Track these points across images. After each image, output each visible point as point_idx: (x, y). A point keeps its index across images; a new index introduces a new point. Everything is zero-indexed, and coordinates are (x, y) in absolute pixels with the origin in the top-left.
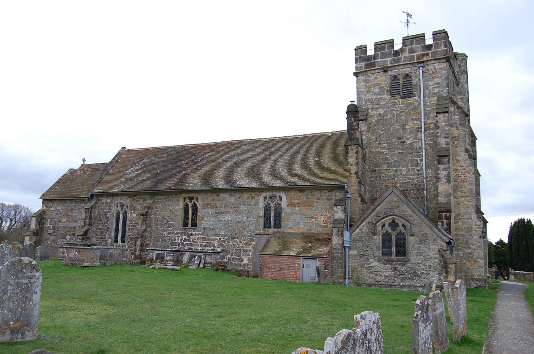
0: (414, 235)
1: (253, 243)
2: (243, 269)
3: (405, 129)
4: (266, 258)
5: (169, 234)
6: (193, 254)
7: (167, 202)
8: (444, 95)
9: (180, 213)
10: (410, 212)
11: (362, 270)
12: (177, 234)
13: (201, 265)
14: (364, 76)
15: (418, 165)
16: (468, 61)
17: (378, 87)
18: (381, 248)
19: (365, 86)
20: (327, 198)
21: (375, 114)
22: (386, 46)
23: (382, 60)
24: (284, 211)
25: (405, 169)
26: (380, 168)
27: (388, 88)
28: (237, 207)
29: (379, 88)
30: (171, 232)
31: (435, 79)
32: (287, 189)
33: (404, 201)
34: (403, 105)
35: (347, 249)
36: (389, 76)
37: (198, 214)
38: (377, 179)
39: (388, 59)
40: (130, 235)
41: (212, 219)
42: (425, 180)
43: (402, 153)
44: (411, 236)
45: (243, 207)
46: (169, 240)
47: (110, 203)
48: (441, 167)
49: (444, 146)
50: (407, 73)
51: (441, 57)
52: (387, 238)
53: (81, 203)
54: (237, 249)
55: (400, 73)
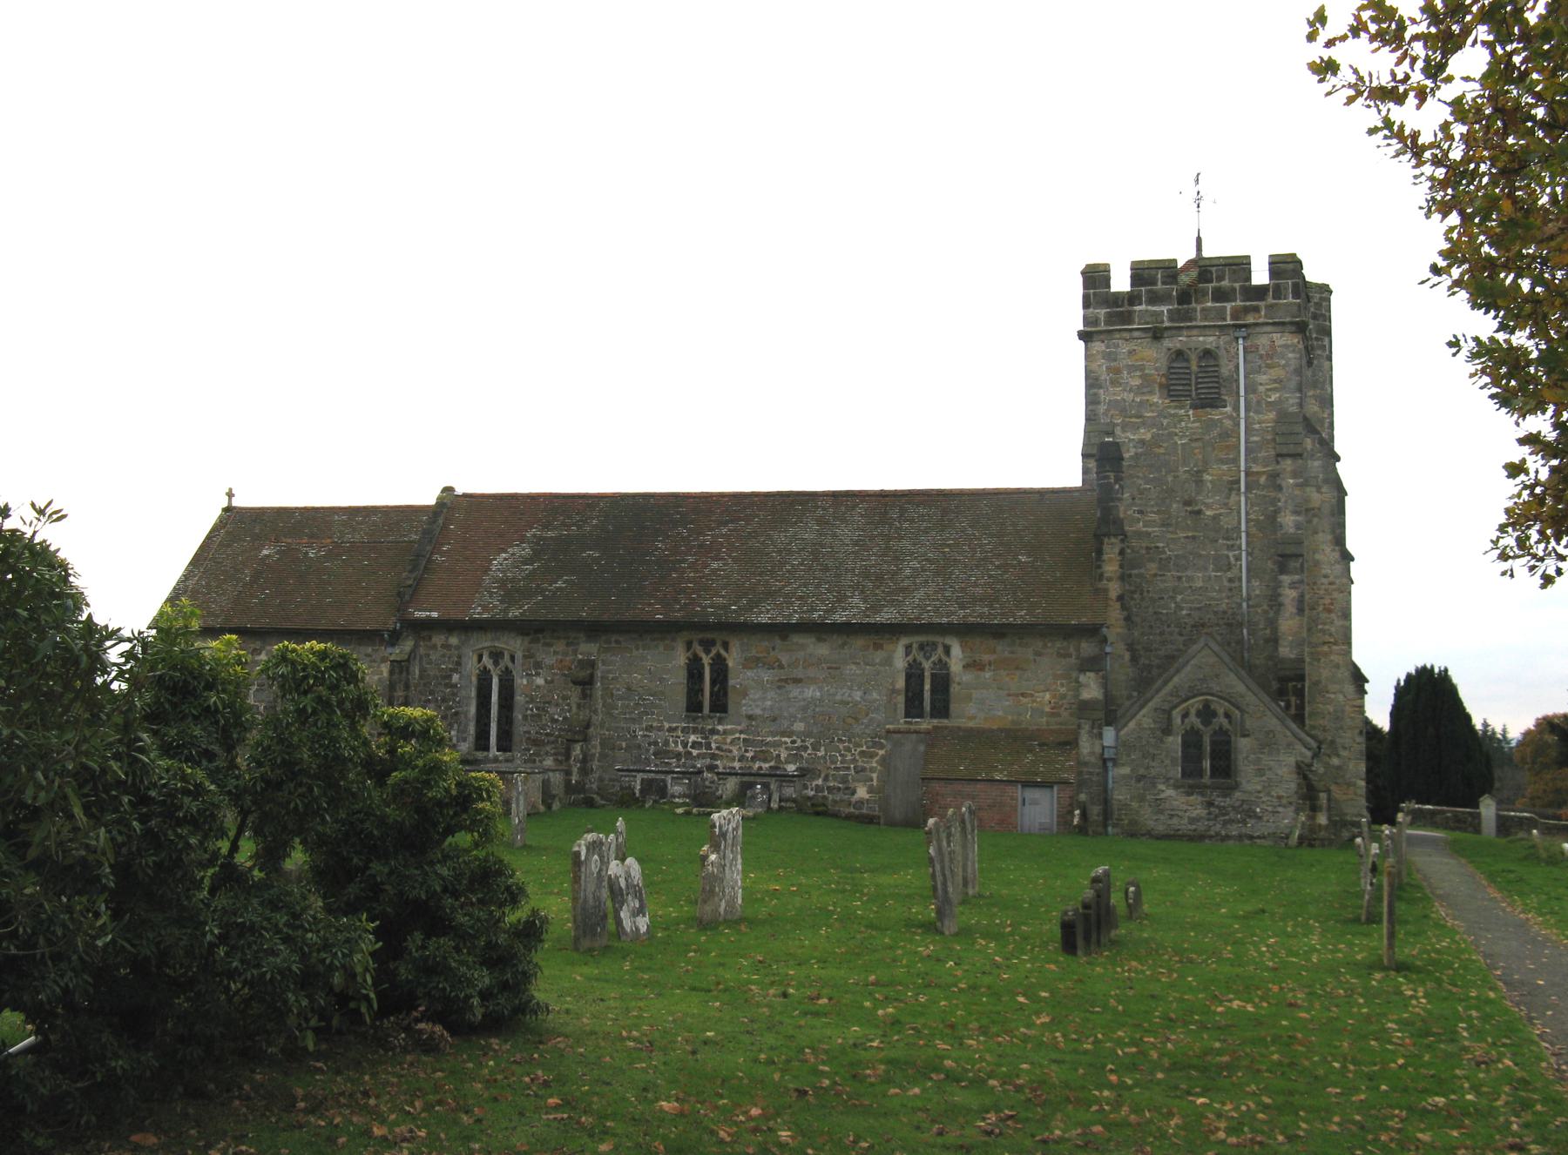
0: (1248, 736)
1: (881, 752)
2: (857, 812)
3: (1202, 481)
4: (936, 786)
5: (646, 730)
6: (746, 779)
7: (637, 649)
8: (1291, 409)
9: (676, 678)
10: (1241, 688)
11: (1140, 806)
12: (671, 730)
13: (774, 805)
14: (1103, 342)
15: (1229, 569)
16: (1333, 298)
17: (1138, 373)
18: (1180, 761)
19: (1107, 368)
20: (1058, 653)
21: (1130, 440)
22: (1159, 276)
23: (1150, 308)
24: (957, 679)
25: (1200, 575)
26: (1142, 571)
27: (1163, 380)
28: (836, 668)
29: (1141, 377)
30: (655, 724)
31: (1272, 371)
32: (964, 631)
33: (1231, 666)
34: (1197, 425)
35: (1110, 764)
36: (1164, 350)
37: (731, 682)
38: (1136, 596)
39: (1165, 309)
40: (529, 732)
41: (771, 694)
42: (1245, 605)
43: (1194, 538)
44: (1244, 736)
45: (854, 667)
46: (650, 744)
47: (457, 648)
48: (1286, 579)
49: (1292, 531)
50: (1208, 347)
51: (1288, 320)
52: (1192, 742)
53: (360, 645)
54: (839, 765)
55: (1192, 345)
